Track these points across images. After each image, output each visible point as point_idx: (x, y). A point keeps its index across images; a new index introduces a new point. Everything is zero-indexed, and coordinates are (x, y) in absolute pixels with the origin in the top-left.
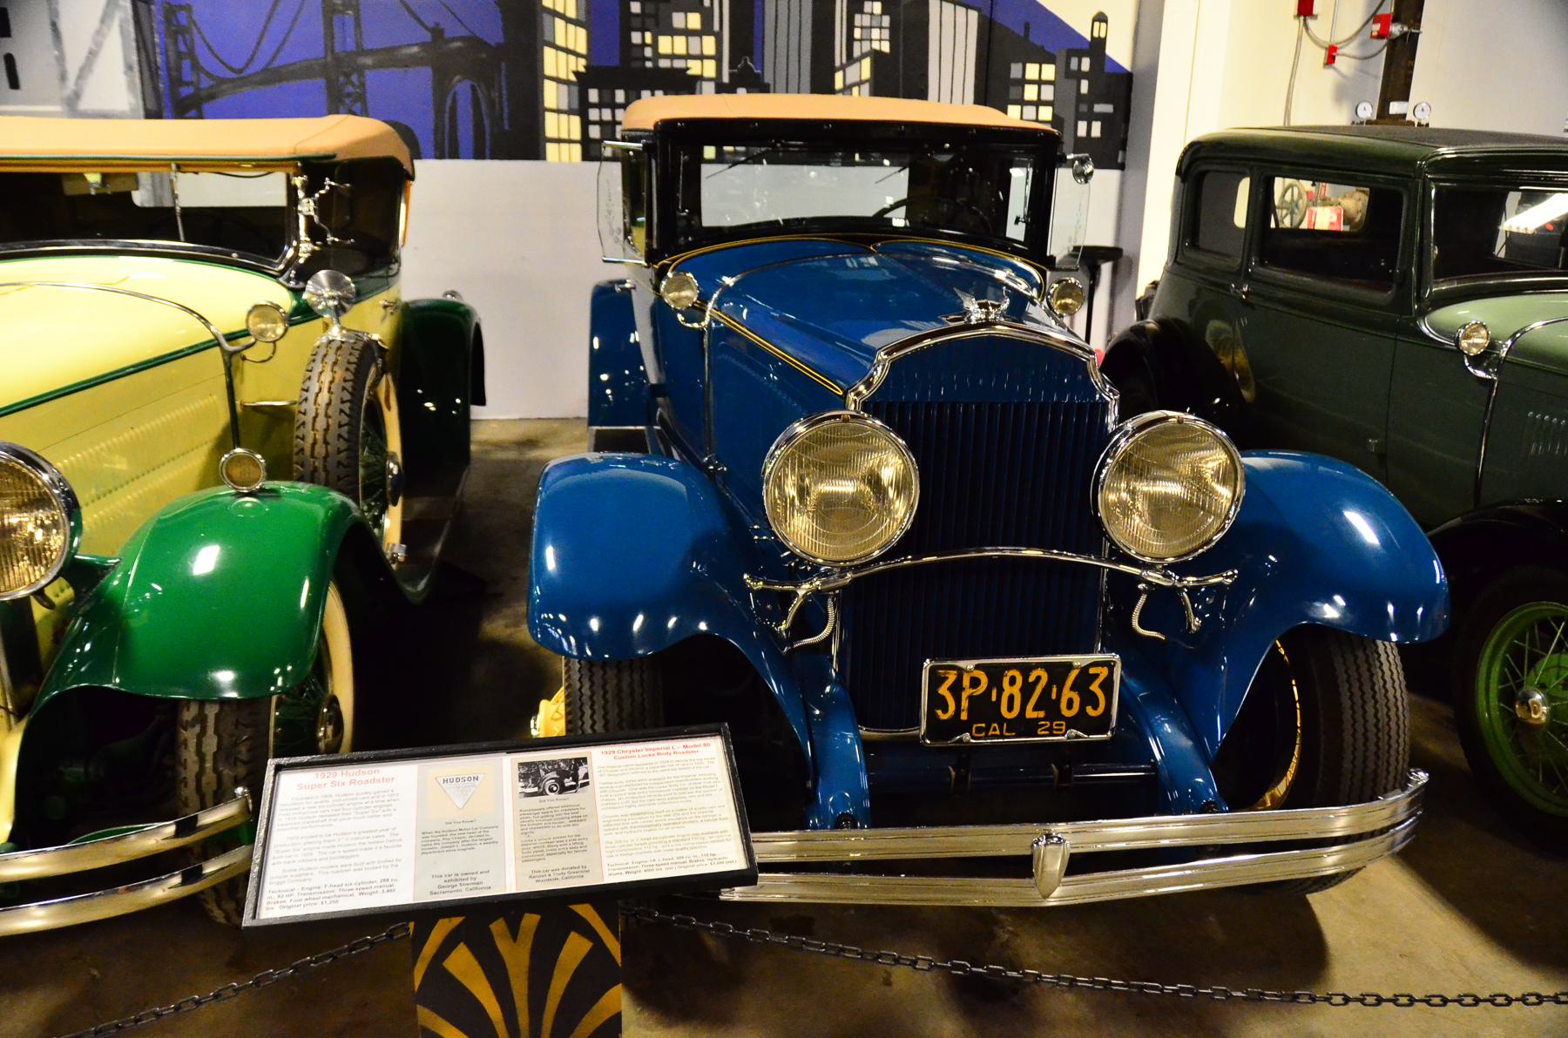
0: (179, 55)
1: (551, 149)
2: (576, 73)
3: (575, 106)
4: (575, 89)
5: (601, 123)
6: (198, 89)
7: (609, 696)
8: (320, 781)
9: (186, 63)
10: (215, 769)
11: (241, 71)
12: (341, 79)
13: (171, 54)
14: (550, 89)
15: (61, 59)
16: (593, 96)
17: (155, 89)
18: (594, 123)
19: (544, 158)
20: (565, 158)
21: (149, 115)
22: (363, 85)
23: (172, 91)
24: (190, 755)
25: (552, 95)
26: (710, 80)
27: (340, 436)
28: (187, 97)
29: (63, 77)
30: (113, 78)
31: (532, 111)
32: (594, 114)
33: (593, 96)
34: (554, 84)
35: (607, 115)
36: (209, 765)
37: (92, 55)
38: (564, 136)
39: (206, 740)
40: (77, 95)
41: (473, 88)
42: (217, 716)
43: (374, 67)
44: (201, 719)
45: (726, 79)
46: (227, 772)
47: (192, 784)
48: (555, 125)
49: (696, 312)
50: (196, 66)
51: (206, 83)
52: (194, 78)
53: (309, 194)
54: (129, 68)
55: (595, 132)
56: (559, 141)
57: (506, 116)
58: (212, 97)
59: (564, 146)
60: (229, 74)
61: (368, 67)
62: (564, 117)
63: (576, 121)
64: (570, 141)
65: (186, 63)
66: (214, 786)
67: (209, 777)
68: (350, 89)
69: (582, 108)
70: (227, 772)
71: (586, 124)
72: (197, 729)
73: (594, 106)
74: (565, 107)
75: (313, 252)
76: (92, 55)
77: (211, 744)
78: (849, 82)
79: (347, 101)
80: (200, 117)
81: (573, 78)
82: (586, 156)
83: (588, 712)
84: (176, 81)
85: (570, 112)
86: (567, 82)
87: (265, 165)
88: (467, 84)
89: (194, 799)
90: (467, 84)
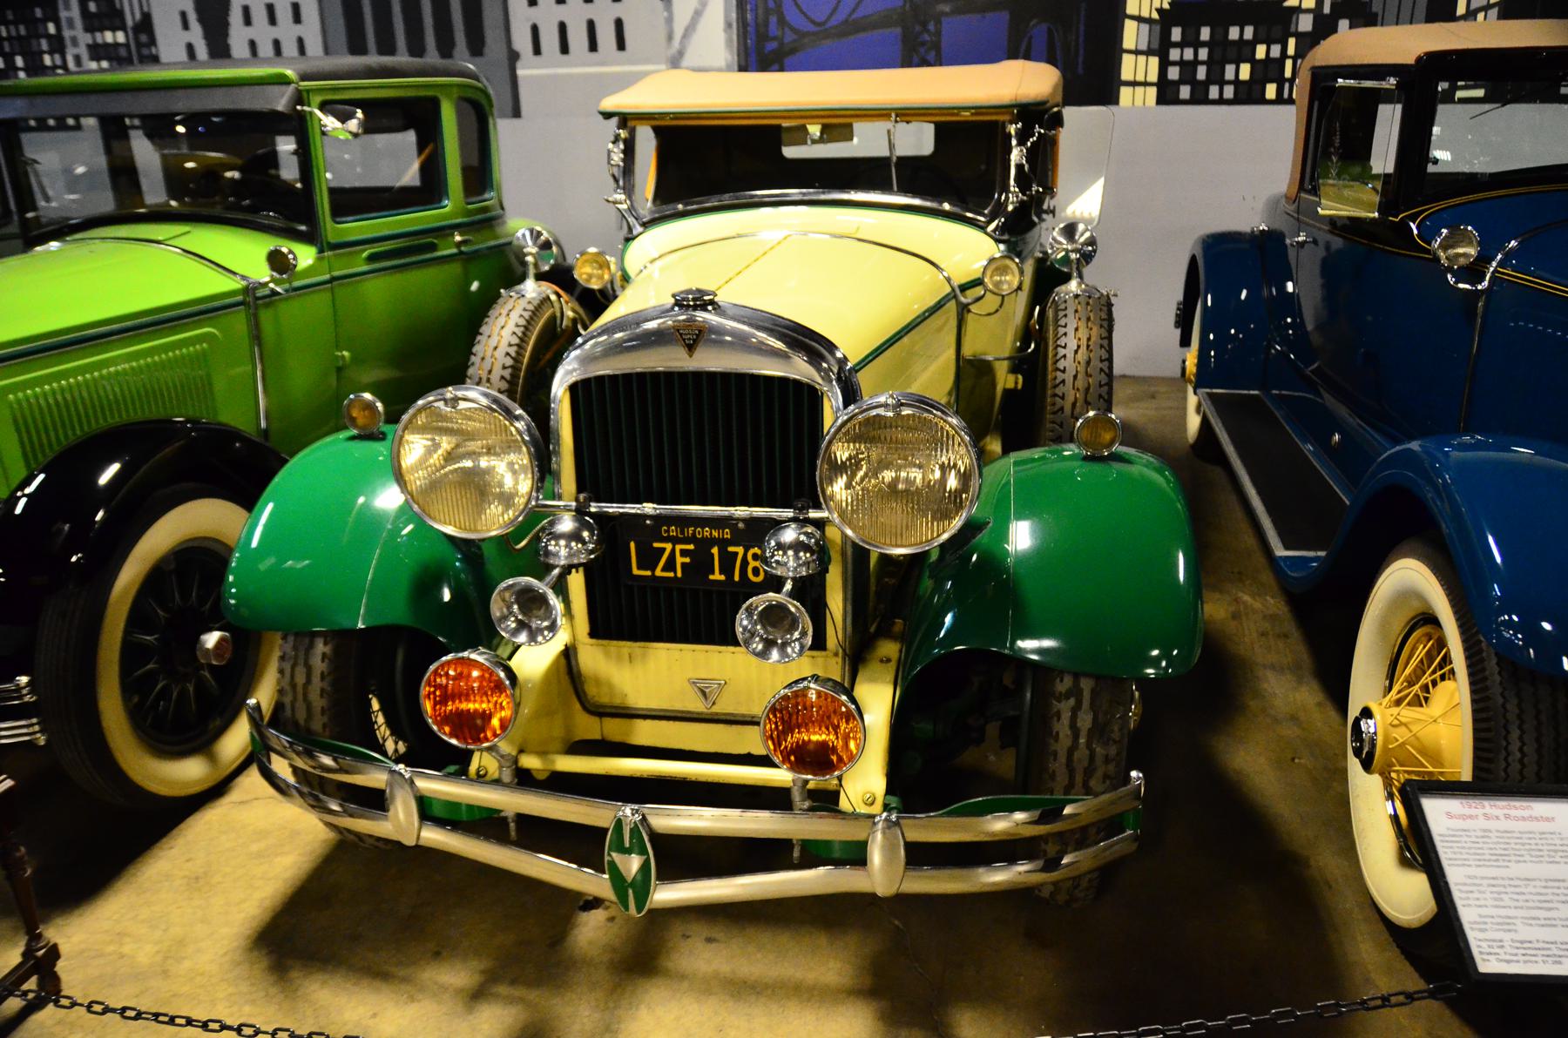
0: (767, 12)
1: (1125, 92)
2: (1160, 11)
3: (1155, 45)
4: (1157, 28)
5: (1182, 63)
6: (782, 44)
7: (1543, 718)
8: (1467, 811)
9: (773, 19)
10: (1089, 745)
11: (824, 23)
12: (918, 28)
13: (760, 11)
14: (1130, 28)
15: (669, 20)
16: (1176, 34)
17: (745, 44)
18: (1174, 63)
19: (1116, 102)
20: (1139, 102)
21: (743, 68)
22: (938, 33)
23: (760, 50)
24: (1062, 727)
25: (1132, 35)
26: (1308, 11)
27: (1100, 396)
28: (773, 51)
29: (670, 37)
30: (715, 35)
31: (1111, 51)
32: (1174, 54)
33: (1176, 34)
34: (1134, 23)
35: (1189, 54)
36: (1082, 741)
37: (698, 14)
38: (1140, 78)
39: (1081, 715)
40: (681, 54)
41: (1050, 31)
42: (1093, 691)
43: (953, 12)
44: (1075, 692)
45: (1327, 10)
46: (1099, 750)
47: (1063, 759)
48: (1130, 67)
49: (1473, 271)
50: (782, 22)
51: (789, 37)
52: (779, 33)
53: (1021, 143)
54: (729, 25)
55: (1173, 73)
56: (1134, 84)
57: (1081, 59)
58: (793, 51)
59: (1139, 90)
60: (813, 28)
61: (946, 14)
62: (1142, 58)
63: (1154, 62)
64: (1145, 84)
65: (773, 19)
66: (1086, 764)
67: (1081, 754)
68: (926, 37)
69: (1160, 49)
70: (1099, 750)
71: (1164, 65)
72: (1072, 701)
73: (1176, 45)
74: (1143, 46)
75: (1022, 203)
76: (698, 14)
77: (1085, 721)
78: (1473, 6)
79: (922, 50)
80: (782, 69)
81: (1155, 16)
82: (1162, 99)
83: (1515, 734)
84: (763, 37)
85: (1149, 53)
86: (1149, 21)
87: (906, 114)
88: (1044, 26)
89: (1062, 778)
90: (1044, 26)
